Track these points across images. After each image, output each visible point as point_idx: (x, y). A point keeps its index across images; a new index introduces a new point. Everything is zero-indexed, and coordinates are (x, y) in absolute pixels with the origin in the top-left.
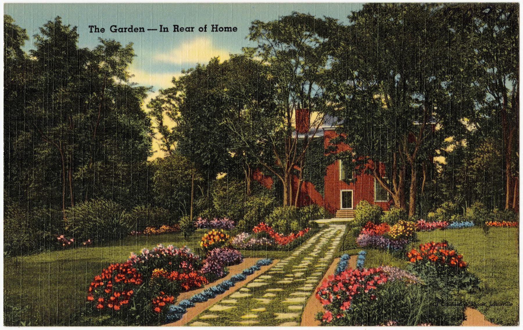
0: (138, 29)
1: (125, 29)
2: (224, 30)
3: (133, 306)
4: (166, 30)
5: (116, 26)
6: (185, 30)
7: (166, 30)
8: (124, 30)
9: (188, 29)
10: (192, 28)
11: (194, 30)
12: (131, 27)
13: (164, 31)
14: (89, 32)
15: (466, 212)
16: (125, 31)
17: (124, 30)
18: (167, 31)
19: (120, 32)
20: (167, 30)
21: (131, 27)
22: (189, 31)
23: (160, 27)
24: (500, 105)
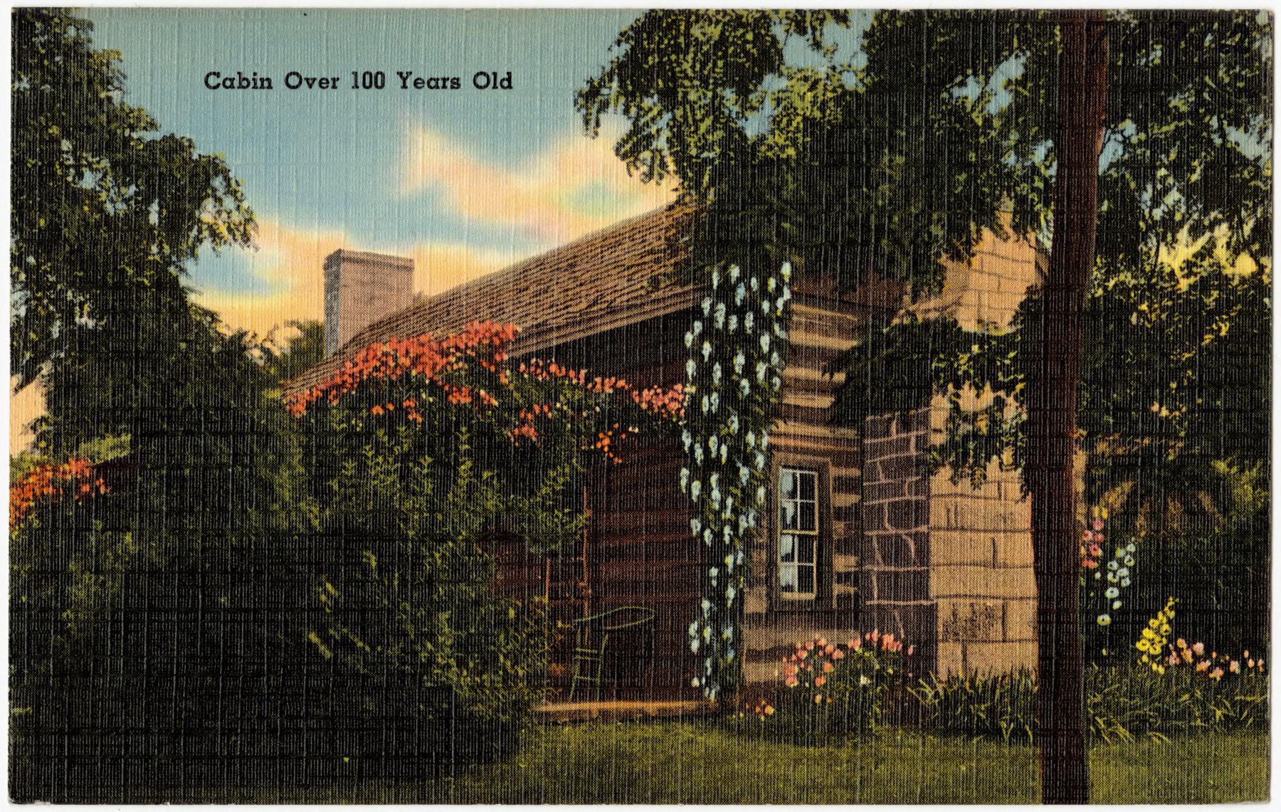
0: (328, 82)
1: (445, 80)
2: (252, 84)
3: (582, 580)
4: (266, 84)
5: (218, 75)
6: (426, 86)
7: (266, 84)
8: (441, 83)
9: (433, 83)
10: (334, 80)
11: (338, 83)
12: (506, 76)
13: (262, 87)
14: (309, 90)
15: (1075, 509)
16: (444, 87)
17: (441, 83)
18: (270, 87)
19: (227, 88)
20: (270, 84)
21: (506, 76)
22: (437, 87)
23: (353, 76)
24: (1089, 444)
